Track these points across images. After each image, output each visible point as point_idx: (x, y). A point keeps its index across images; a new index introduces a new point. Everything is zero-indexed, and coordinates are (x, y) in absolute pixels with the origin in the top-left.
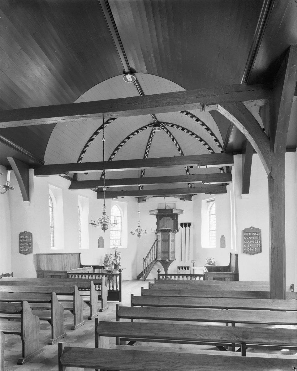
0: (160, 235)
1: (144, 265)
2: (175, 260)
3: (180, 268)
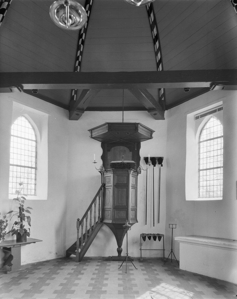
0: (110, 176)
1: (78, 232)
2: (137, 222)
3: (151, 237)
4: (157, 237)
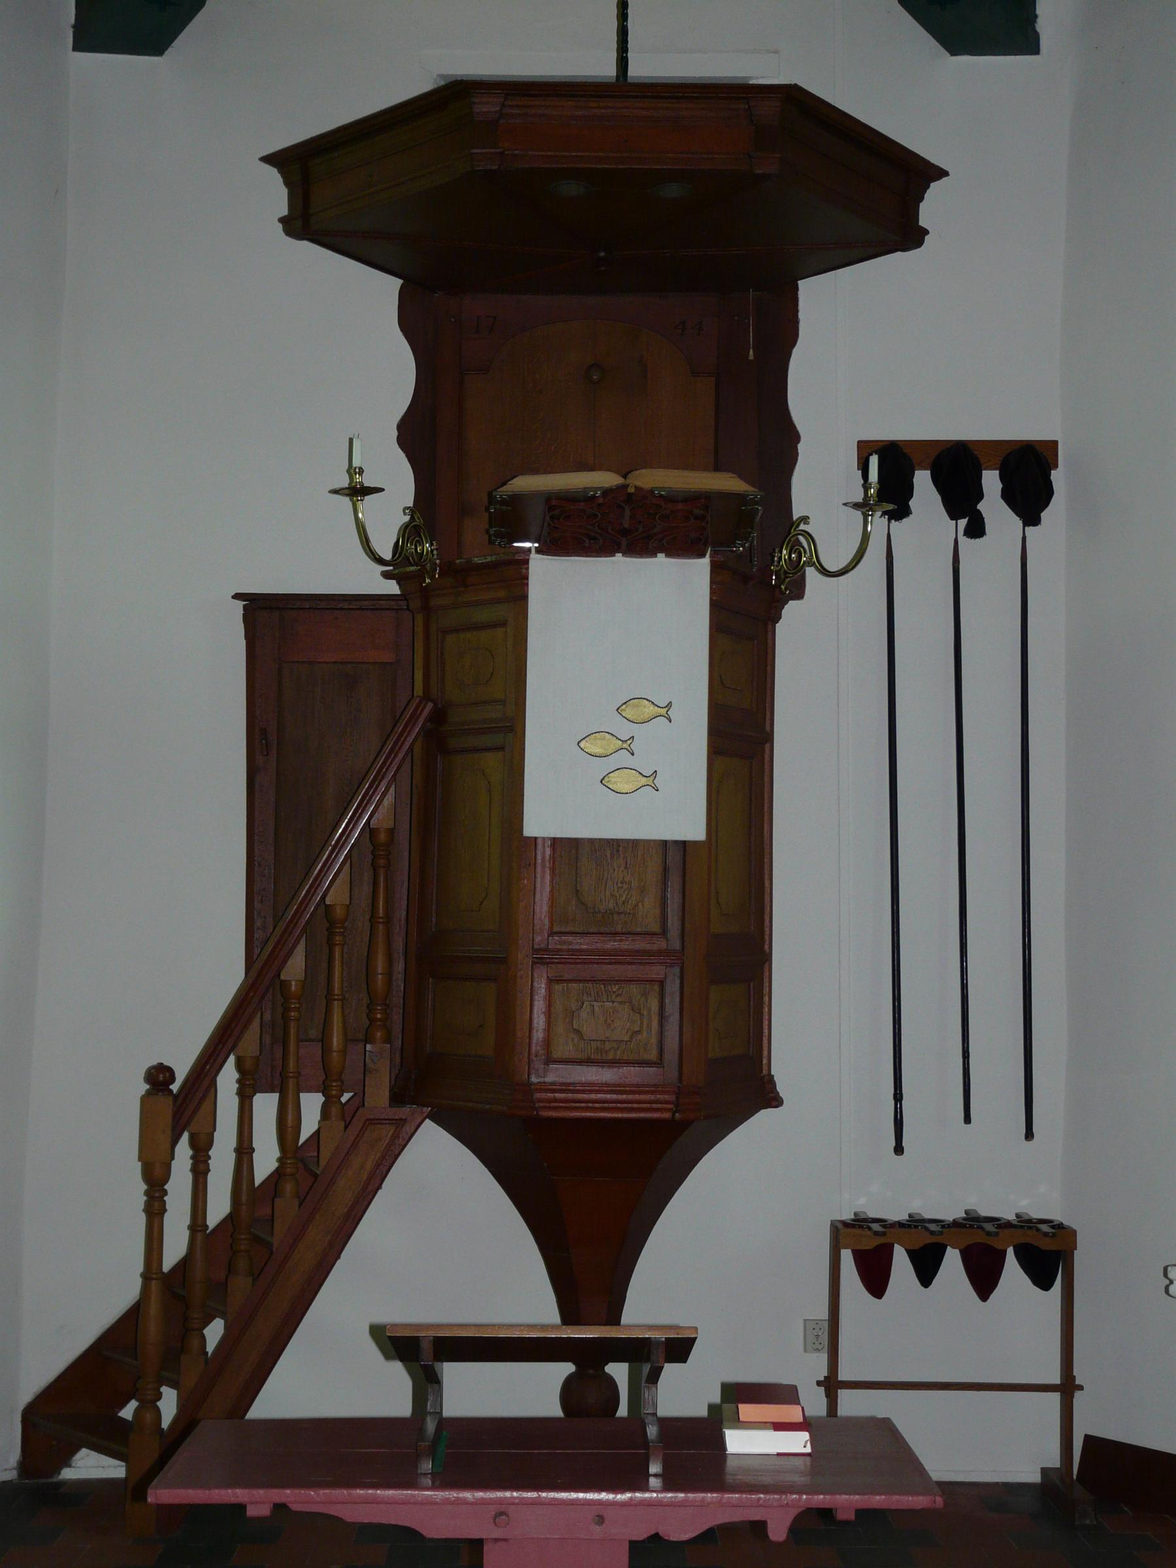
1: (155, 1209)
4: (1010, 1251)
